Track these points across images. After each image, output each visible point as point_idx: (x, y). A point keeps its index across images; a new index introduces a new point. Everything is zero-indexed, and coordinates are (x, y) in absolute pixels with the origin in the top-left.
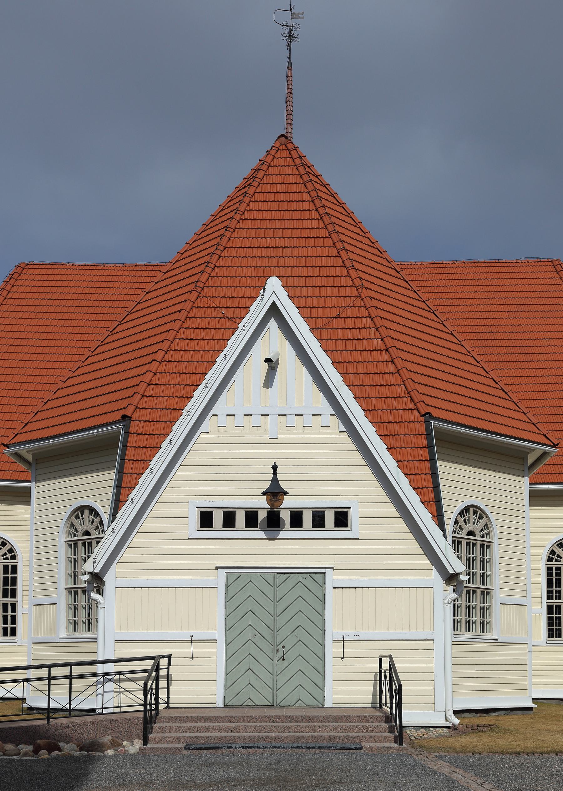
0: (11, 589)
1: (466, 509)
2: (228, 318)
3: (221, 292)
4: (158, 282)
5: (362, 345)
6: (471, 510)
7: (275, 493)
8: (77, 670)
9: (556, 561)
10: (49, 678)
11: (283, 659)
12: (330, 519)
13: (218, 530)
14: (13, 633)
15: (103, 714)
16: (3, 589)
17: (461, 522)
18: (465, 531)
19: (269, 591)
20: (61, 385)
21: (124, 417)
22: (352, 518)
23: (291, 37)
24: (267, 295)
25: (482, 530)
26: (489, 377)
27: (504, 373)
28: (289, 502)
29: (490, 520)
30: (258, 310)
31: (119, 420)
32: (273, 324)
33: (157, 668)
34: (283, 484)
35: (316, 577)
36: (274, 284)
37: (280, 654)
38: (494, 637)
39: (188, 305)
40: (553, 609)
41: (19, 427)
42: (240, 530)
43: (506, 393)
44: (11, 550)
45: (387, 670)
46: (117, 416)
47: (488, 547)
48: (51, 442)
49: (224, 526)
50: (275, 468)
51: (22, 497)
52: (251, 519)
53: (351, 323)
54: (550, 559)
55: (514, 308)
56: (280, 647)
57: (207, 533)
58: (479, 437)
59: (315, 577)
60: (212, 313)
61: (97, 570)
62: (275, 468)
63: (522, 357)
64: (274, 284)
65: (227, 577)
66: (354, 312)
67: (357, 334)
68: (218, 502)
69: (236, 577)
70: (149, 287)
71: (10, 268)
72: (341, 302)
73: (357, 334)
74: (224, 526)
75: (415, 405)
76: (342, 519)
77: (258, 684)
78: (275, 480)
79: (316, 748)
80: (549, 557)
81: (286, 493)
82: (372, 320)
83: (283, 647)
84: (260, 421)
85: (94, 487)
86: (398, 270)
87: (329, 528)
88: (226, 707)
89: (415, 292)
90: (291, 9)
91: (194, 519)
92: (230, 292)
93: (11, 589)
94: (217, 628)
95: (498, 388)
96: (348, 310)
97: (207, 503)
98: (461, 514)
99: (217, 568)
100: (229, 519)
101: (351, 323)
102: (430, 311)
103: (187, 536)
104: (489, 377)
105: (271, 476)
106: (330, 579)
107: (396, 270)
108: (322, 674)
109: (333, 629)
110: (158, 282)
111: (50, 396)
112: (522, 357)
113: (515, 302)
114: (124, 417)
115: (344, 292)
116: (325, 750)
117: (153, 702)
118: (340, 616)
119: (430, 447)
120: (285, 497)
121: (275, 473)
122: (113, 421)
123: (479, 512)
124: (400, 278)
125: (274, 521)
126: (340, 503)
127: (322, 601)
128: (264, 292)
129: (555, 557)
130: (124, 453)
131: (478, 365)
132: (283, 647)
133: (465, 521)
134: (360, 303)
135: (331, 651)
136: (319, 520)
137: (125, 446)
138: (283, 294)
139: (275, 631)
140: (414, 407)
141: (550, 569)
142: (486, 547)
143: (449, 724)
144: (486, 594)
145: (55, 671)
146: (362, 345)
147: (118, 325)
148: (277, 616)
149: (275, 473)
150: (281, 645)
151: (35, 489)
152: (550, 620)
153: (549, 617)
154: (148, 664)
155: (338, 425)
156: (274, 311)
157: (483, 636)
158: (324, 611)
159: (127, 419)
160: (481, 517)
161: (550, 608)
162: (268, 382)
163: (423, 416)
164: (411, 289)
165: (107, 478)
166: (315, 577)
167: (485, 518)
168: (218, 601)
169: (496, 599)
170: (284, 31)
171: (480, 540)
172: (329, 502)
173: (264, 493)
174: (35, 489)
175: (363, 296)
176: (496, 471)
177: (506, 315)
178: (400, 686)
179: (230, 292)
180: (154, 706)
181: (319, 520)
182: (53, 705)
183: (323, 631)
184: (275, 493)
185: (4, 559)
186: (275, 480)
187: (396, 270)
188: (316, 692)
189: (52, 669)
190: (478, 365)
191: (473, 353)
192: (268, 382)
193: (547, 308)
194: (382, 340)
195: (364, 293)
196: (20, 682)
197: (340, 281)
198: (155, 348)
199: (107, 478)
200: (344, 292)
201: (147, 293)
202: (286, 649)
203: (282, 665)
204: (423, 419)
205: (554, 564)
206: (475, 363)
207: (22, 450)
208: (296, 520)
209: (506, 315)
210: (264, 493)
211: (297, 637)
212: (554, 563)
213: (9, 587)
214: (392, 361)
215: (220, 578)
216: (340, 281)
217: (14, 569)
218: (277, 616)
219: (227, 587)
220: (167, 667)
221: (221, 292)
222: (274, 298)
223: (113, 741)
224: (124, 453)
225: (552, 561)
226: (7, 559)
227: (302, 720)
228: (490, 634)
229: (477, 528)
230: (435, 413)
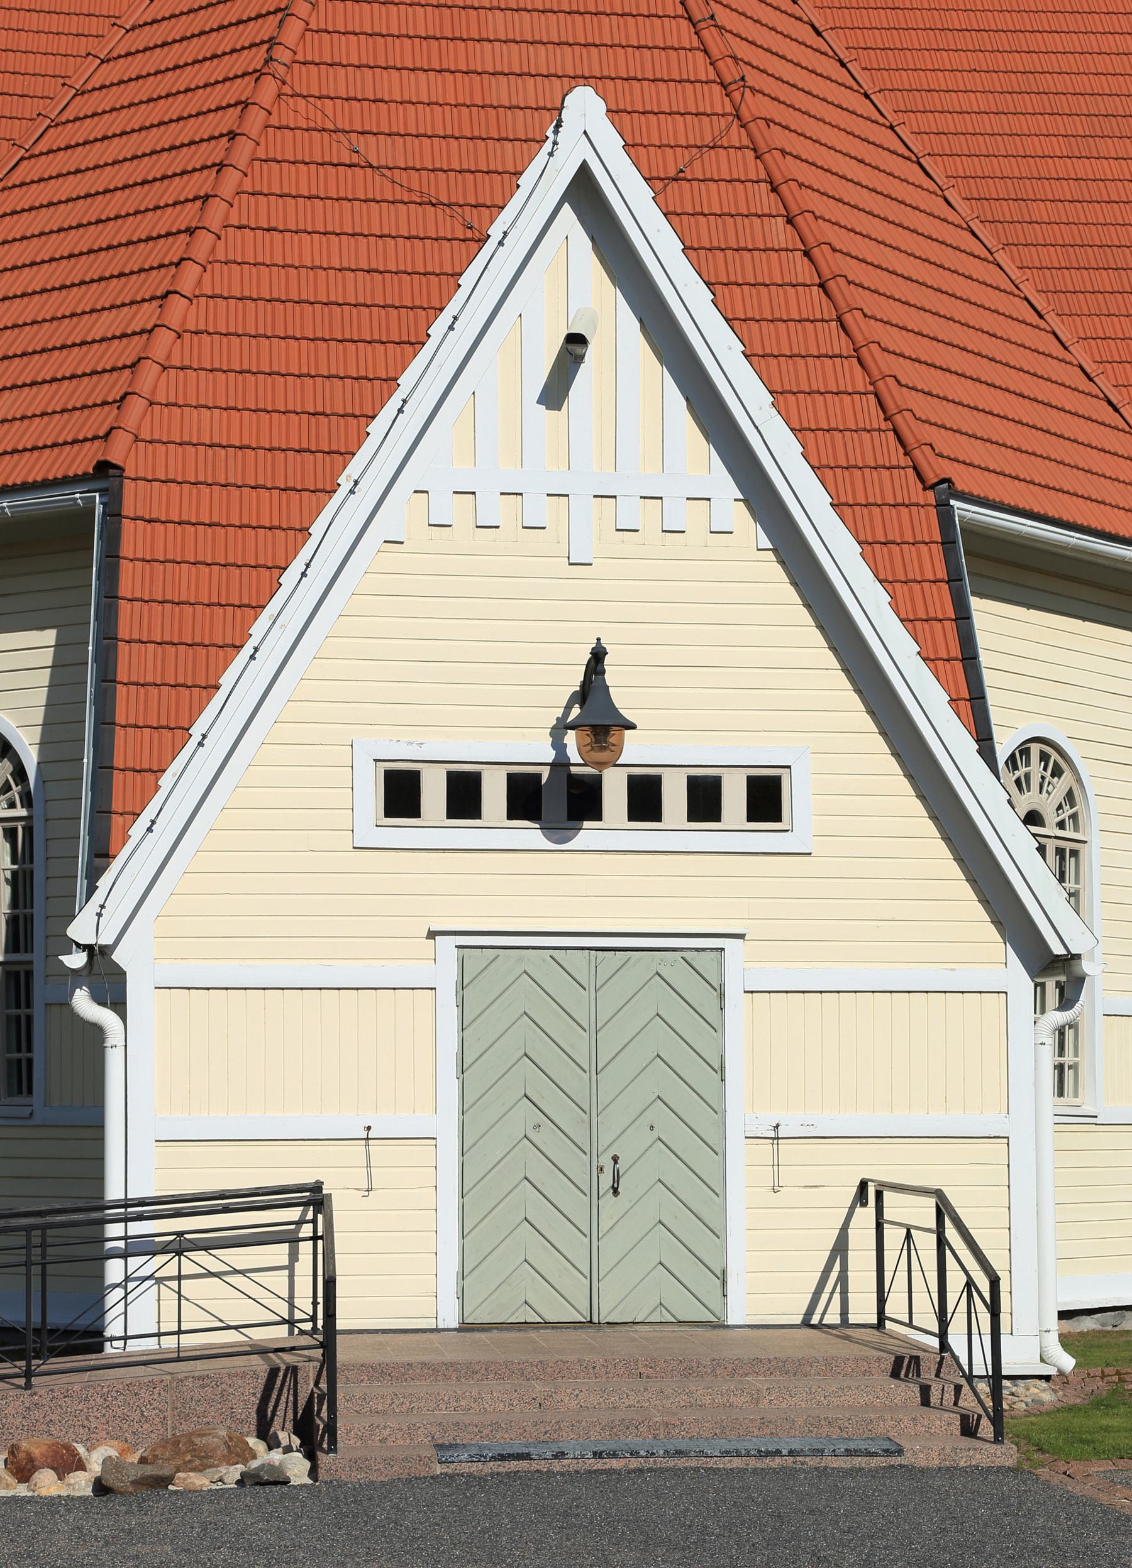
2: (371, 166)
3: (340, 82)
4: (133, 28)
7: (595, 712)
15: (179, 1357)
19: (576, 1001)
21: (104, 468)
22: (796, 797)
25: (1060, 807)
26: (1070, 363)
28: (637, 750)
29: (1079, 780)
30: (546, 178)
31: (85, 474)
35: (697, 959)
36: (585, 108)
37: (607, 1180)
38: (1087, 1109)
43: (1116, 410)
46: (83, 461)
47: (1075, 853)
49: (451, 814)
52: (525, 797)
55: (1079, 126)
57: (403, 832)
58: (1066, 547)
59: (691, 966)
60: (319, 147)
61: (106, 939)
62: (598, 656)
64: (585, 108)
66: (720, 164)
68: (436, 745)
69: (485, 954)
74: (451, 814)
75: (906, 454)
76: (765, 799)
77: (550, 1263)
79: (785, 1452)
81: (632, 727)
82: (774, 190)
83: (615, 1159)
84: (539, 510)
88: (465, 1328)
89: (867, 96)
92: (367, 83)
95: (1096, 397)
96: (706, 156)
97: (403, 751)
99: (432, 935)
102: (908, 159)
104: (1070, 363)
106: (740, 967)
107: (813, 26)
108: (719, 1233)
109: (745, 1108)
110: (133, 28)
113: (1082, 105)
114: (104, 468)
115: (689, 97)
116: (807, 1459)
118: (766, 1069)
119: (954, 579)
120: (628, 733)
122: (65, 477)
123: (1054, 756)
124: (826, 54)
125: (583, 801)
126: (763, 754)
127: (717, 1028)
128: (556, 132)
131: (1042, 324)
132: (615, 1159)
133: (1018, 782)
134: (736, 136)
135: (743, 1166)
137: (112, 556)
138: (610, 142)
139: (591, 1112)
140: (904, 461)
143: (1051, 1371)
147: (22, 159)
148: (593, 1069)
155: (749, 533)
156: (584, 193)
158: (722, 1058)
159: (111, 472)
160: (1057, 772)
162: (555, 393)
163: (932, 487)
164: (856, 87)
166: (691, 966)
167: (1067, 774)
168: (432, 1031)
171: (1056, 837)
175: (746, 115)
176: (1029, 606)
177: (1057, 146)
179: (367, 83)
181: (704, 800)
183: (719, 1111)
184: (595, 712)
187: (813, 26)
188: (707, 1286)
190: (1042, 324)
191: (1028, 290)
192: (555, 393)
194: (807, 254)
195: (754, 105)
200: (689, 97)
201: (103, 62)
203: (610, 1206)
204: (931, 496)
206: (1033, 318)
208: (645, 800)
209: (1057, 146)
211: (652, 1128)
214: (839, 319)
215: (443, 965)
218: (593, 1069)
219: (462, 986)
221: (340, 82)
223: (231, 1439)
227: (714, 1370)
228: (1076, 1101)
230: (964, 480)
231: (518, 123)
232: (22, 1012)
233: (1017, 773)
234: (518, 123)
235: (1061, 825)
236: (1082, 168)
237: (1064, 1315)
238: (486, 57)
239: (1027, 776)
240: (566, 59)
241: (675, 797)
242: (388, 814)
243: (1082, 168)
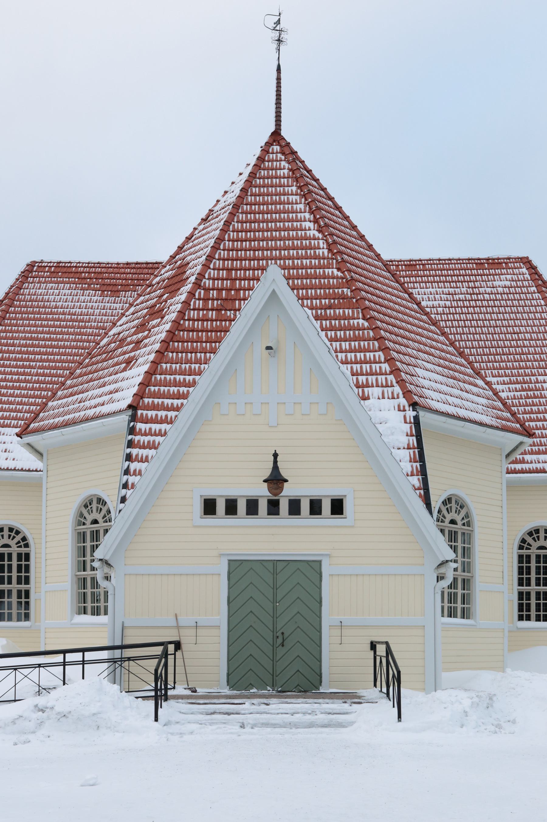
0: (25, 576)
1: (449, 500)
7: (276, 480)
8: (89, 656)
9: (527, 549)
10: (64, 664)
11: (283, 646)
13: (220, 520)
16: (18, 576)
17: (445, 512)
18: (447, 521)
22: (348, 507)
25: (463, 519)
28: (289, 491)
33: (165, 654)
34: (284, 473)
37: (280, 641)
40: (523, 595)
42: (242, 521)
45: (384, 657)
50: (275, 455)
52: (252, 507)
56: (279, 634)
57: (210, 520)
62: (275, 455)
65: (229, 564)
68: (221, 491)
71: (22, 267)
76: (338, 507)
78: (275, 467)
80: (520, 545)
81: (286, 481)
83: (283, 633)
86: (386, 265)
90: (280, 14)
91: (199, 507)
93: (25, 576)
94: (220, 616)
97: (210, 493)
98: (444, 503)
100: (231, 507)
105: (271, 465)
117: (163, 687)
121: (275, 462)
126: (337, 493)
129: (526, 545)
132: (283, 633)
133: (447, 509)
136: (315, 508)
141: (520, 557)
145: (70, 657)
149: (275, 462)
150: (281, 631)
153: (519, 603)
154: (159, 650)
160: (462, 507)
161: (520, 594)
170: (273, 35)
172: (326, 491)
173: (265, 481)
178: (399, 672)
180: (163, 692)
181: (315, 508)
184: (276, 480)
185: (18, 547)
186: (275, 467)
189: (67, 655)
196: (36, 667)
202: (286, 635)
205: (524, 552)
208: (295, 507)
210: (265, 481)
212: (524, 551)
213: (23, 574)
217: (27, 557)
220: (173, 653)
222: (273, 287)
225: (523, 549)
226: (20, 547)
232: (106, 604)
233: (447, 507)
235: (464, 524)
239: (451, 507)
241: (305, 507)
242: (205, 514)
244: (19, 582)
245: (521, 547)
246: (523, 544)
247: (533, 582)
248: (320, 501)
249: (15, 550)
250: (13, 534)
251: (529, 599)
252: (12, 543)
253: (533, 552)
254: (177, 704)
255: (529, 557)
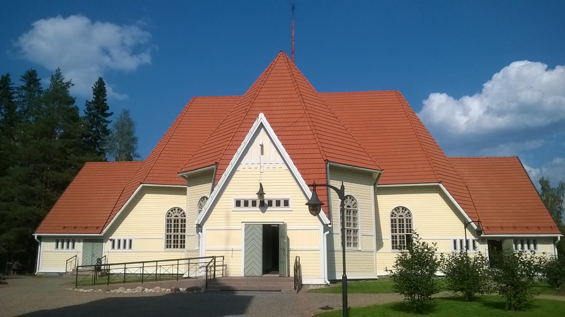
5: (304, 133)
6: (349, 197)
7: (261, 193)
12: (282, 203)
13: (242, 208)
14: (184, 248)
20: (199, 149)
22: (290, 203)
23: (293, 8)
24: (259, 120)
27: (363, 141)
32: (262, 130)
36: (261, 115)
38: (360, 249)
39: (242, 118)
41: (182, 166)
42: (250, 208)
44: (184, 213)
48: (193, 172)
51: (183, 191)
53: (301, 124)
54: (392, 216)
57: (238, 209)
63: (382, 131)
64: (261, 115)
66: (303, 120)
67: (303, 128)
68: (242, 197)
70: (232, 110)
72: (298, 116)
73: (303, 128)
76: (286, 203)
85: (204, 189)
87: (282, 208)
88: (245, 276)
91: (233, 203)
94: (241, 245)
97: (239, 197)
100: (246, 204)
101: (301, 124)
103: (231, 210)
111: (195, 153)
112: (382, 131)
126: (286, 197)
130: (215, 177)
141: (392, 220)
142: (355, 212)
144: (356, 231)
146: (304, 133)
151: (189, 189)
152: (393, 241)
157: (355, 249)
160: (353, 200)
161: (393, 236)
165: (210, 185)
169: (359, 234)
172: (281, 197)
174: (189, 189)
182: (144, 273)
184: (261, 193)
192: (262, 154)
193: (393, 110)
197: (298, 108)
198: (229, 135)
199: (210, 185)
207: (184, 174)
215: (243, 226)
216: (298, 108)
222: (261, 121)
224: (215, 177)
229: (351, 205)
230: (329, 159)
231: (253, 117)
234: (253, 117)
236: (380, 116)
237: (131, 241)
238: (274, 108)
240: (260, 109)
243: (380, 116)
244: (400, 232)
245: (168, 216)
246: (168, 215)
247: (398, 231)
248: (256, 201)
249: (180, 218)
250: (174, 211)
251: (177, 238)
252: (404, 214)
253: (173, 218)
254: (330, 305)
255: (395, 220)
